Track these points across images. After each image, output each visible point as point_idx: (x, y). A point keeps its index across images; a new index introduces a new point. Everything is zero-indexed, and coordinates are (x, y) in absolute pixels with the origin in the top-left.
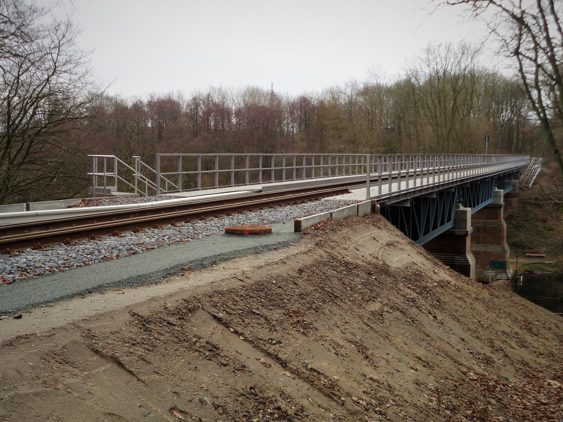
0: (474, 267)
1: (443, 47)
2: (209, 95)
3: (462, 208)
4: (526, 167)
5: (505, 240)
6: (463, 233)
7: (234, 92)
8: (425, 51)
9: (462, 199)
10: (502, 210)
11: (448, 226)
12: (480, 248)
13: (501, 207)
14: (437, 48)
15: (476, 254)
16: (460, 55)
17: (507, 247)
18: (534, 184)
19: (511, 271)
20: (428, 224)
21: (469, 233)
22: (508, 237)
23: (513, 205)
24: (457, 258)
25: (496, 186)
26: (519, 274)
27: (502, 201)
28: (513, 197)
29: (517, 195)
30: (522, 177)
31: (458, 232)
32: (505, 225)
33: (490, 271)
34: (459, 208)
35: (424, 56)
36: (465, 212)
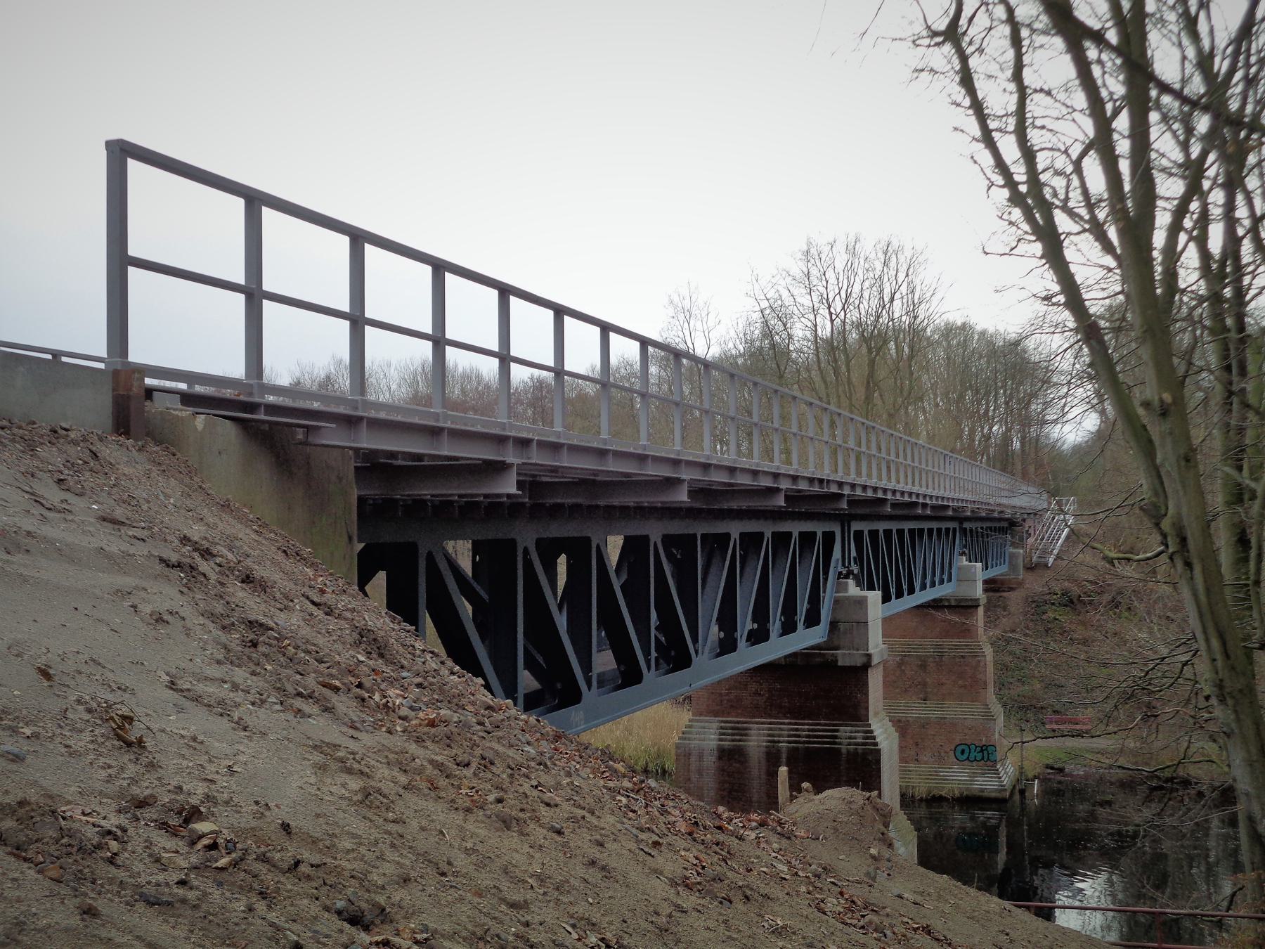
0: (896, 757)
1: (840, 247)
2: (328, 377)
3: (853, 589)
4: (1036, 514)
5: (991, 689)
6: (859, 662)
7: (393, 374)
8: (799, 255)
9: (856, 570)
10: (981, 610)
11: (806, 638)
12: (916, 710)
13: (977, 606)
14: (826, 249)
15: (902, 727)
16: (879, 266)
17: (997, 709)
18: (1058, 557)
19: (1011, 769)
20: (727, 619)
21: (875, 660)
22: (1001, 686)
23: (1012, 610)
24: (845, 731)
25: (963, 553)
26: (1030, 775)
27: (978, 592)
28: (1011, 589)
29: (1020, 584)
30: (1031, 540)
31: (845, 658)
32: (988, 651)
33: (956, 769)
34: (846, 590)
35: (797, 268)
36: (862, 602)
